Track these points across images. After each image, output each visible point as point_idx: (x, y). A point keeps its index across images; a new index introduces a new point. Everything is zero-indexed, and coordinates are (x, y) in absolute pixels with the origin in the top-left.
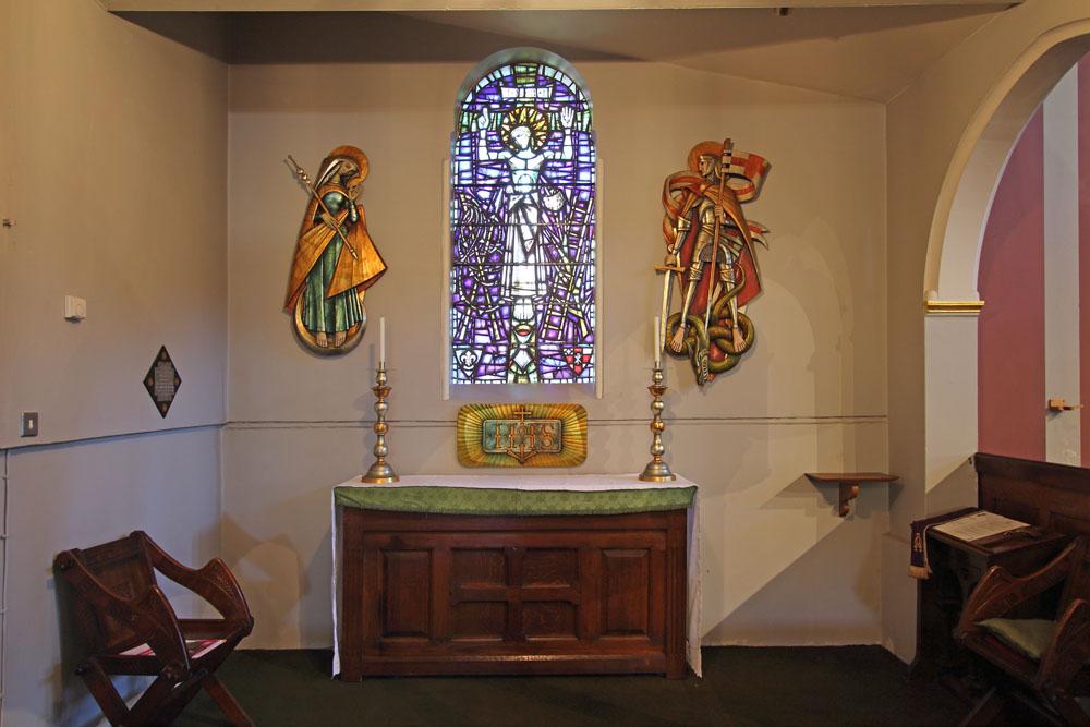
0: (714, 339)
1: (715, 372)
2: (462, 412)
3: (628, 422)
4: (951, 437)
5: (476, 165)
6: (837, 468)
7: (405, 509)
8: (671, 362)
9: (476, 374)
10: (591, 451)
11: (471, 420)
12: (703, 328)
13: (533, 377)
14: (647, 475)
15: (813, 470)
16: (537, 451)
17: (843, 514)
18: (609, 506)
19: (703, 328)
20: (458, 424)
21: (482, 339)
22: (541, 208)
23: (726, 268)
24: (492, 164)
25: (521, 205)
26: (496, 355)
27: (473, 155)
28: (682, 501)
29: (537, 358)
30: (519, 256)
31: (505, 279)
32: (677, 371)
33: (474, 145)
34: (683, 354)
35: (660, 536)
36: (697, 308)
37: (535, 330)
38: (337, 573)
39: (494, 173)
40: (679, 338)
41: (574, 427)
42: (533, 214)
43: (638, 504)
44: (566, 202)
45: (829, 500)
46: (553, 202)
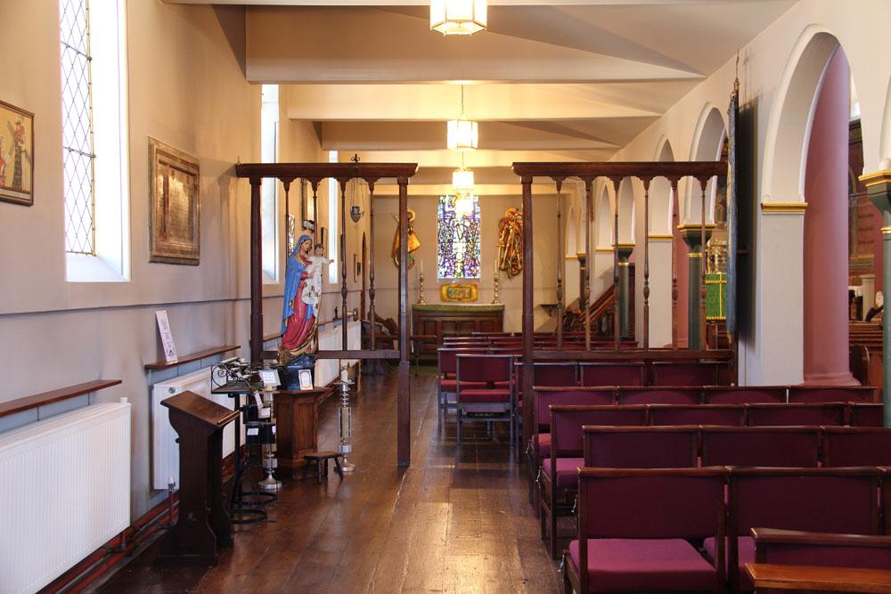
0: (513, 266)
1: (514, 275)
2: (442, 286)
3: (489, 289)
4: (572, 294)
5: (445, 212)
6: (548, 303)
7: (735, 273)
8: (501, 273)
9: (445, 275)
10: (479, 297)
11: (444, 289)
12: (510, 262)
13: (462, 276)
14: (494, 303)
15: (542, 303)
16: (464, 297)
17: (550, 315)
18: (482, 310)
19: (510, 262)
20: (441, 289)
21: (447, 264)
22: (464, 226)
23: (516, 246)
24: (449, 212)
25: (458, 225)
26: (451, 269)
27: (444, 209)
28: (501, 308)
29: (463, 270)
30: (457, 240)
31: (454, 247)
32: (502, 274)
33: (444, 206)
34: (504, 270)
35: (497, 315)
36: (508, 257)
37: (463, 262)
38: (733, 235)
39: (450, 215)
40: (503, 266)
41: (474, 291)
42: (461, 227)
43: (490, 309)
44: (471, 224)
45: (547, 311)
46: (468, 224)
